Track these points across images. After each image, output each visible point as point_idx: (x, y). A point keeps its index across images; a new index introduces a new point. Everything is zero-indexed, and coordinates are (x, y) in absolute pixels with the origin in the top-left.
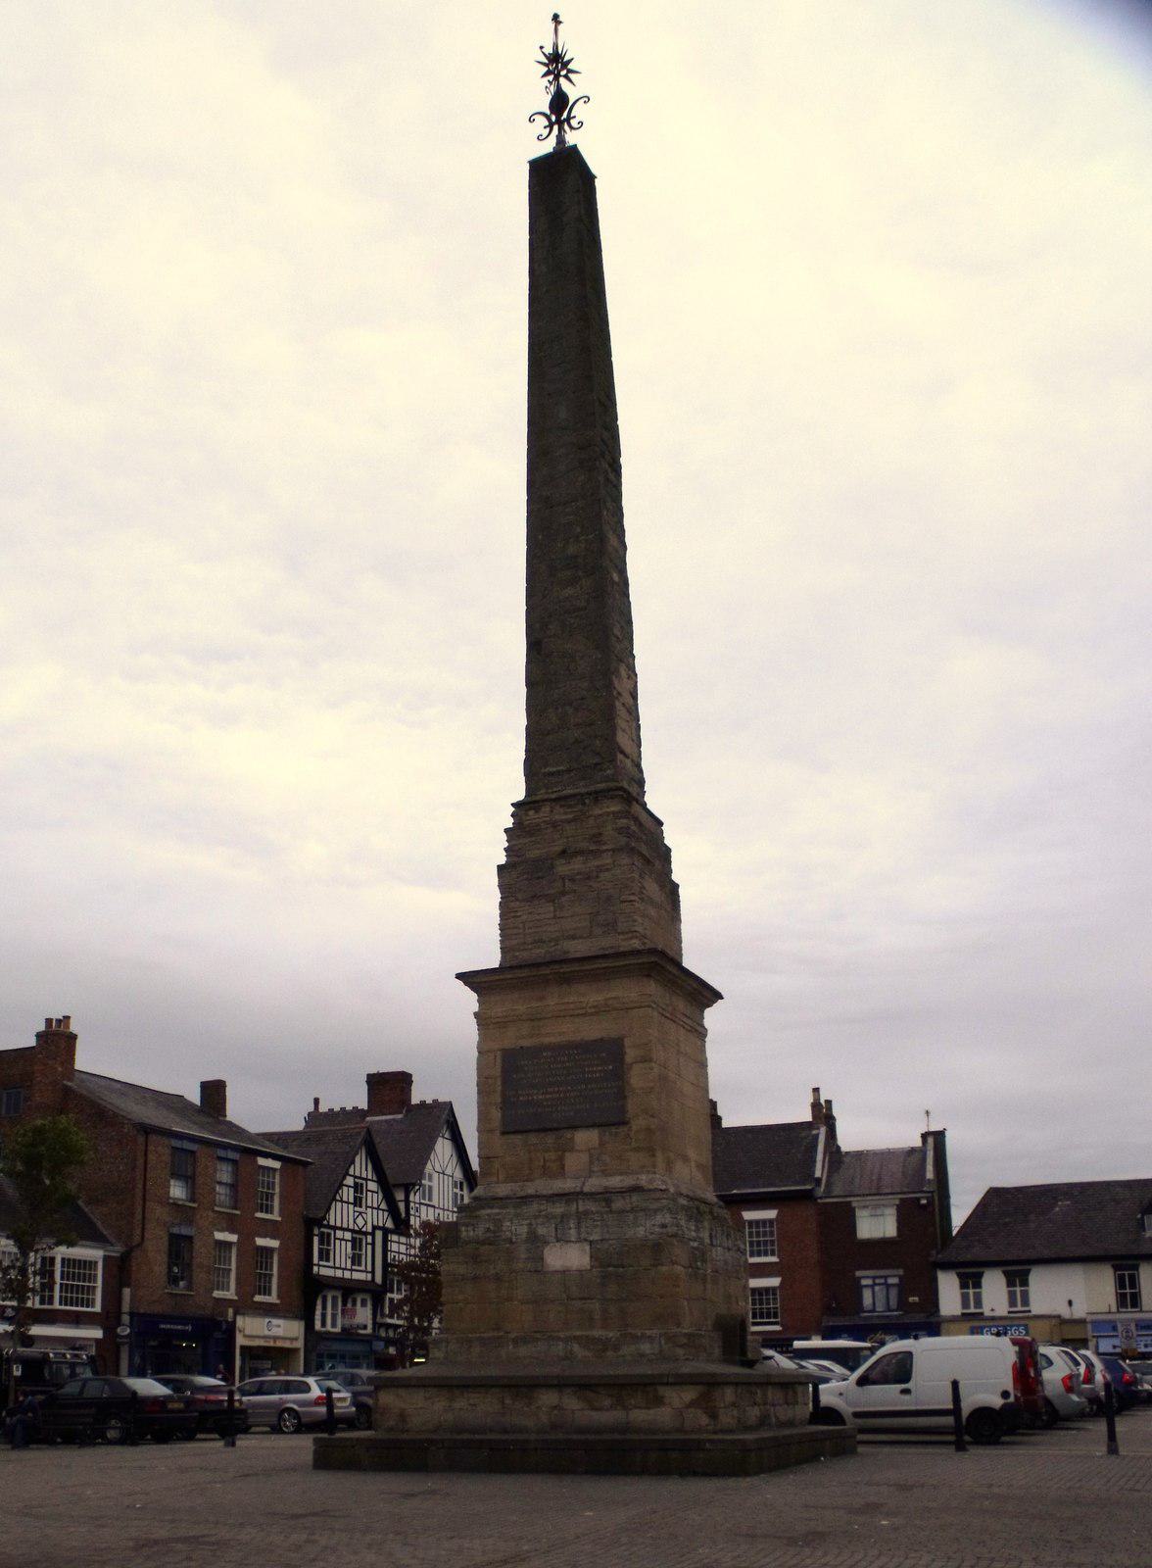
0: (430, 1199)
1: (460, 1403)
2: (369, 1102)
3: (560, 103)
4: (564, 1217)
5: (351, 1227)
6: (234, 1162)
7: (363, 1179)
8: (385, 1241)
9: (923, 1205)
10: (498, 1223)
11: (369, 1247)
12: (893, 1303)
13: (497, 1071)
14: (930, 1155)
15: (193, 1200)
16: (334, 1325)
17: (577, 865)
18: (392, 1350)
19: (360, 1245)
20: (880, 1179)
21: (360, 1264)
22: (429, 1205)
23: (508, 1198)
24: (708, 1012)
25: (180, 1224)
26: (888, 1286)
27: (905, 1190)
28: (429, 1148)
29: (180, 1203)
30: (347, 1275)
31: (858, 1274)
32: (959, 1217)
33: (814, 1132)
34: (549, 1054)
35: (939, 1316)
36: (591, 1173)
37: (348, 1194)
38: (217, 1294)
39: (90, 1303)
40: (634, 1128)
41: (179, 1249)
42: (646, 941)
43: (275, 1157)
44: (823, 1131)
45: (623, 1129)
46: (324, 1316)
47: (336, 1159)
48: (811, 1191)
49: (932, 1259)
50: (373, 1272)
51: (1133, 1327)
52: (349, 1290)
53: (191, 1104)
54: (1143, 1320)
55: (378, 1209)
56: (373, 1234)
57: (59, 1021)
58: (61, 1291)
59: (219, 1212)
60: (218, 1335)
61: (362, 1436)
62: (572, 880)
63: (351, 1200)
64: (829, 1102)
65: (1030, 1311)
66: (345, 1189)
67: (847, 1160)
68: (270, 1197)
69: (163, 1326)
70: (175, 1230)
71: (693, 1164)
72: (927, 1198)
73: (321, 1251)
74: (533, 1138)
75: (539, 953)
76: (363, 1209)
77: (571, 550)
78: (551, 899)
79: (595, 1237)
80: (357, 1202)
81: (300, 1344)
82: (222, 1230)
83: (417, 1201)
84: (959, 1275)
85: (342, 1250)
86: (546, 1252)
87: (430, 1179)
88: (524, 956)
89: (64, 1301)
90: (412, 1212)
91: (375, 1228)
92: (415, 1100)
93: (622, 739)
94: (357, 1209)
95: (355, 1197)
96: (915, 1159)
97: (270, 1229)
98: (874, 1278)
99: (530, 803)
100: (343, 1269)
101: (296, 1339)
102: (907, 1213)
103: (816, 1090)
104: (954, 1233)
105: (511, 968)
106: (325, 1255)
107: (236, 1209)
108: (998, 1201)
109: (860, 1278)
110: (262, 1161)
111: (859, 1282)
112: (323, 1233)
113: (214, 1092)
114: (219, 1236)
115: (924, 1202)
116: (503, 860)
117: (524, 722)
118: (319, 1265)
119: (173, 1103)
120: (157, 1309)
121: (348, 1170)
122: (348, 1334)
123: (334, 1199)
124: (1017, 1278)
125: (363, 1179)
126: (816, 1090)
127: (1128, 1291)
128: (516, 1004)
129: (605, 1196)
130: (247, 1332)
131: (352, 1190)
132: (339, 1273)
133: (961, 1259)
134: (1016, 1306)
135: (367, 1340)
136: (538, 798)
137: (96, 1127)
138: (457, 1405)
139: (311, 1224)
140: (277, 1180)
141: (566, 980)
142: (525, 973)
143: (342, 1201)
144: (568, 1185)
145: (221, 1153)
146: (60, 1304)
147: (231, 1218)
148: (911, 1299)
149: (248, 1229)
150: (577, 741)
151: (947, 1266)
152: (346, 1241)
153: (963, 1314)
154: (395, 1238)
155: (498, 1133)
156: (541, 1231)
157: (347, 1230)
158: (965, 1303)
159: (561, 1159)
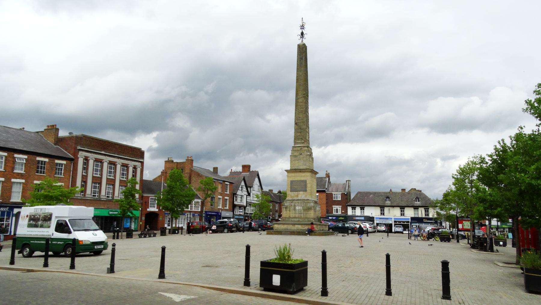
2: (242, 170)
3: (302, 34)
6: (221, 183)
8: (247, 197)
18: (247, 218)
30: (240, 204)
31: (333, 206)
39: (199, 209)
44: (327, 179)
45: (306, 192)
48: (325, 190)
52: (240, 207)
53: (212, 172)
64: (329, 173)
68: (227, 189)
72: (347, 193)
74: (294, 192)
80: (242, 190)
82: (219, 196)
85: (239, 199)
89: (194, 209)
97: (227, 195)
102: (343, 195)
106: (236, 200)
115: (346, 194)
123: (238, 190)
124: (362, 208)
128: (291, 174)
132: (238, 203)
134: (362, 214)
139: (234, 195)
141: (300, 172)
144: (299, 199)
151: (349, 206)
154: (248, 197)
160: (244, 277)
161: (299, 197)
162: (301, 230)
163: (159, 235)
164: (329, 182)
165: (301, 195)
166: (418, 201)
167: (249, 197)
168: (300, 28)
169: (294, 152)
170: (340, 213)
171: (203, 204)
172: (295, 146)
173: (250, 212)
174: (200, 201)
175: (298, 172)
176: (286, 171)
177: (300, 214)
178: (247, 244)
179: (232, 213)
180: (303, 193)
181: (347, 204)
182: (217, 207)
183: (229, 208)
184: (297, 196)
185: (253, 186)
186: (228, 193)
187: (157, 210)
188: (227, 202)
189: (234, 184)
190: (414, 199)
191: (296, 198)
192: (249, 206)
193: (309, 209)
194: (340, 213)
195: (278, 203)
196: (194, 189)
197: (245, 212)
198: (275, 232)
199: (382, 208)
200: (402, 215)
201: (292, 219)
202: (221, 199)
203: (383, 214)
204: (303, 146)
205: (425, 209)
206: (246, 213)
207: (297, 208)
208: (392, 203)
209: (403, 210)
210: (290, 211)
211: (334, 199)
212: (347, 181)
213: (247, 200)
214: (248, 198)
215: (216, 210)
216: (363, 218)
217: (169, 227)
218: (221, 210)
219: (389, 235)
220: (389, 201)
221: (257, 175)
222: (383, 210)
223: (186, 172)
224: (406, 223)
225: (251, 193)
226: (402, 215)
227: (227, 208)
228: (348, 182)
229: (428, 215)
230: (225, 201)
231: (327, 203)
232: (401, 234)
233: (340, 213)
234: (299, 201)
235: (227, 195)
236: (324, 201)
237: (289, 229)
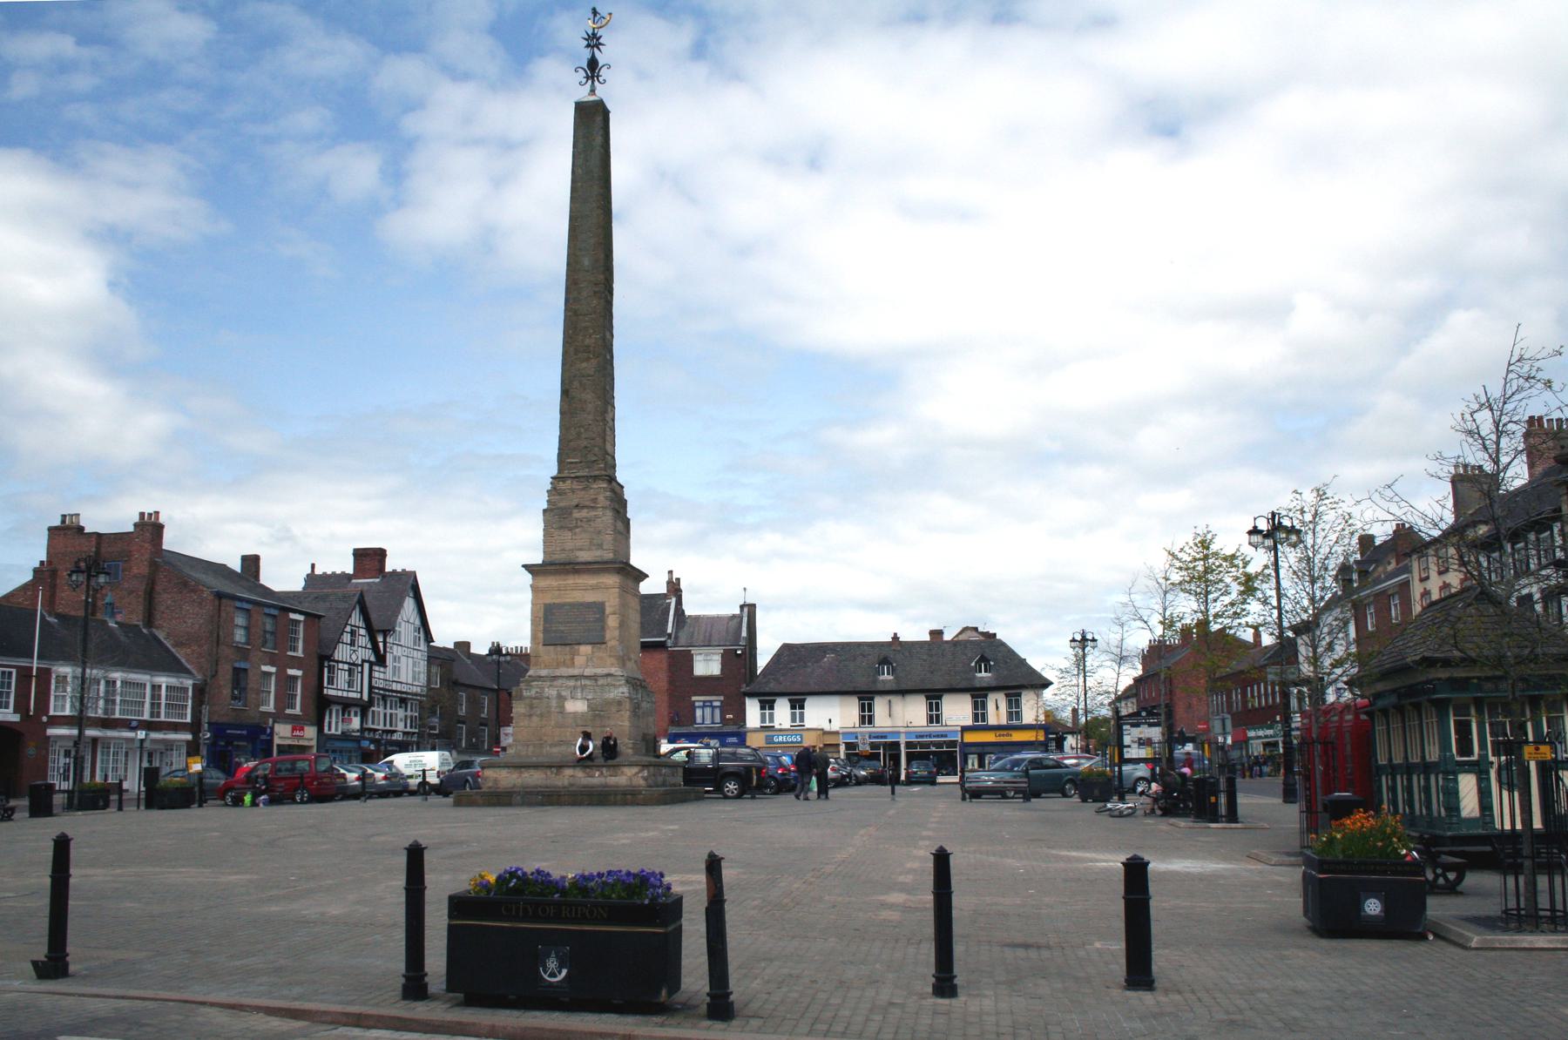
0: (399, 641)
1: (526, 775)
3: (593, 65)
4: (575, 687)
5: (348, 661)
8: (371, 671)
10: (542, 688)
11: (360, 675)
12: (718, 719)
13: (541, 614)
14: (745, 620)
15: (248, 644)
16: (336, 730)
17: (584, 513)
18: (372, 747)
19: (334, 670)
20: (711, 635)
21: (333, 684)
22: (398, 645)
23: (547, 677)
24: (641, 584)
25: (240, 661)
26: (713, 708)
27: (728, 644)
28: (400, 605)
29: (240, 646)
30: (345, 694)
31: (694, 698)
32: (762, 662)
33: (668, 601)
36: (587, 666)
39: (184, 715)
41: (239, 675)
43: (301, 613)
44: (673, 601)
45: (604, 646)
46: (330, 723)
47: (339, 613)
49: (742, 690)
50: (361, 692)
51: (867, 737)
52: (346, 705)
53: (233, 572)
54: (874, 733)
55: (365, 648)
56: (362, 666)
57: (150, 515)
59: (266, 652)
60: (263, 737)
62: (581, 521)
63: (349, 642)
64: (678, 579)
67: (688, 621)
69: (229, 731)
70: (237, 665)
71: (633, 661)
73: (329, 677)
74: (559, 648)
76: (355, 648)
77: (587, 341)
78: (570, 529)
79: (589, 697)
80: (352, 643)
81: (314, 743)
83: (391, 641)
84: (790, 700)
85: (342, 677)
86: (566, 703)
87: (400, 627)
89: (167, 715)
90: (388, 650)
91: (363, 661)
92: (388, 568)
93: (608, 447)
95: (351, 640)
96: (735, 622)
97: (296, 663)
98: (704, 702)
101: (311, 739)
102: (728, 659)
103: (670, 572)
104: (759, 672)
106: (331, 681)
107: (275, 649)
108: (789, 654)
109: (694, 701)
111: (694, 704)
114: (265, 668)
115: (739, 652)
116: (545, 506)
117: (558, 433)
118: (328, 688)
119: (221, 570)
120: (224, 720)
122: (345, 736)
123: (339, 642)
124: (797, 704)
126: (670, 572)
127: (866, 713)
128: (547, 582)
129: (594, 678)
130: (281, 735)
131: (349, 635)
132: (340, 693)
133: (762, 691)
135: (357, 740)
136: (563, 475)
137: (181, 593)
138: (523, 775)
139: (322, 659)
142: (558, 567)
143: (343, 643)
144: (576, 672)
145: (238, 604)
146: (120, 714)
148: (728, 716)
149: (282, 662)
150: (586, 447)
151: (752, 695)
153: (762, 727)
154: (376, 668)
156: (564, 693)
158: (763, 720)
159: (573, 659)
160: (401, 966)
163: (132, 808)
164: (679, 611)
166: (986, 671)
167: (382, 669)
168: (586, 43)
173: (385, 725)
174: (189, 683)
175: (567, 572)
176: (528, 567)
178: (410, 842)
180: (593, 652)
182: (258, 706)
183: (301, 711)
185: (397, 629)
186: (300, 653)
187: (16, 718)
188: (294, 688)
190: (973, 664)
192: (381, 703)
195: (492, 690)
196: (168, 636)
197: (365, 726)
198: (483, 795)
199: (866, 698)
200: (931, 722)
202: (273, 678)
203: (867, 718)
205: (1007, 695)
206: (370, 730)
209: (937, 704)
213: (374, 680)
214: (376, 674)
217: (65, 786)
218: (271, 720)
219: (896, 792)
220: (888, 674)
221: (409, 586)
222: (870, 705)
223: (135, 571)
224: (918, 750)
225: (388, 654)
226: (931, 722)
227: (297, 710)
228: (746, 610)
229: (1018, 715)
230: (286, 683)
232: (928, 788)
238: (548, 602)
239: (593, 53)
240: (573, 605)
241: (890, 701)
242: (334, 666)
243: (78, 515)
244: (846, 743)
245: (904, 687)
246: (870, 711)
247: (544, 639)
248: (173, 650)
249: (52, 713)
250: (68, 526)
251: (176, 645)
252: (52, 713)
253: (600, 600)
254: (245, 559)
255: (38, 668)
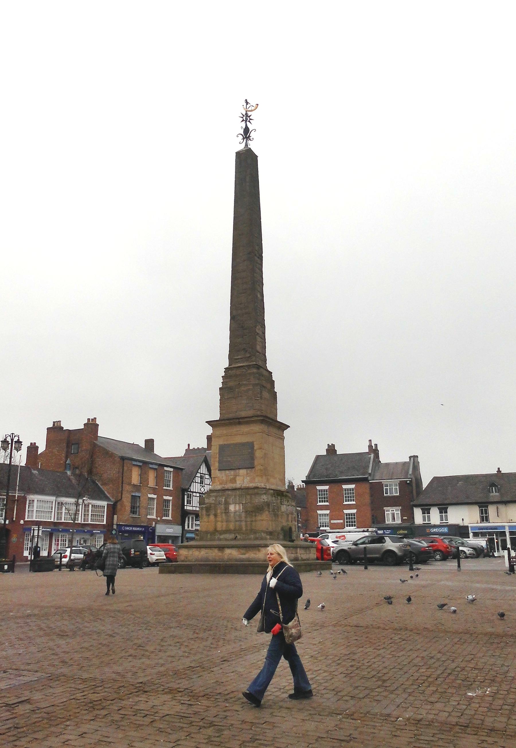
3: (247, 130)
5: (199, 492)
6: (155, 469)
7: (204, 474)
9: (408, 483)
16: (192, 527)
31: (385, 508)
34: (233, 446)
35: (415, 524)
37: (198, 480)
38: (149, 517)
40: (257, 469)
42: (262, 411)
43: (171, 467)
44: (372, 456)
57: (92, 419)
58: (91, 517)
61: (26, 514)
64: (376, 445)
65: (430, 523)
66: (197, 478)
74: (227, 472)
75: (231, 416)
80: (202, 482)
88: (226, 416)
94: (201, 485)
95: (201, 481)
97: (168, 493)
99: (229, 368)
100: (196, 507)
102: (403, 485)
103: (370, 441)
105: (222, 420)
106: (189, 502)
110: (166, 468)
112: (188, 494)
113: (150, 443)
114: (150, 496)
115: (408, 482)
116: (221, 386)
118: (187, 506)
119: (134, 447)
121: (198, 471)
124: (443, 510)
125: (204, 474)
128: (223, 431)
132: (194, 509)
134: (484, 521)
140: (172, 475)
141: (240, 423)
145: (135, 463)
147: (154, 489)
151: (417, 506)
152: (197, 497)
155: (217, 470)
157: (198, 493)
161: (238, 482)
162: (236, 560)
165: (242, 478)
169: (228, 380)
170: (398, 521)
171: (113, 510)
172: (231, 367)
175: (235, 424)
177: (237, 523)
179: (180, 527)
180: (247, 474)
181: (412, 503)
184: (234, 481)
186: (171, 488)
188: (168, 506)
189: (184, 472)
191: (230, 486)
193: (259, 509)
194: (400, 522)
201: (221, 534)
203: (485, 518)
204: (247, 366)
207: (232, 508)
208: (502, 495)
210: (216, 515)
211: (385, 495)
212: (410, 457)
215: (143, 522)
216: (446, 530)
218: (154, 523)
220: (496, 492)
230: (163, 505)
231: (372, 503)
233: (400, 522)
234: (238, 492)
235: (168, 493)
236: (367, 499)
237: (210, 558)
238: (221, 443)
239: (246, 125)
240: (236, 445)
241: (497, 508)
242: (191, 494)
243: (60, 421)
244: (473, 532)
245: (505, 499)
246: (486, 513)
247: (219, 466)
248: (101, 487)
249: (26, 519)
250: (56, 427)
251: (102, 485)
252: (26, 519)
253: (251, 440)
254: (147, 441)
255: (18, 496)
